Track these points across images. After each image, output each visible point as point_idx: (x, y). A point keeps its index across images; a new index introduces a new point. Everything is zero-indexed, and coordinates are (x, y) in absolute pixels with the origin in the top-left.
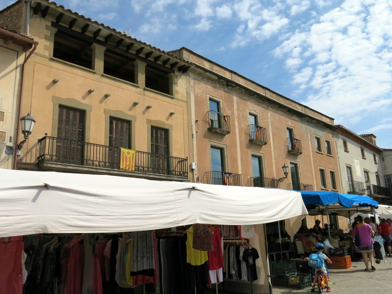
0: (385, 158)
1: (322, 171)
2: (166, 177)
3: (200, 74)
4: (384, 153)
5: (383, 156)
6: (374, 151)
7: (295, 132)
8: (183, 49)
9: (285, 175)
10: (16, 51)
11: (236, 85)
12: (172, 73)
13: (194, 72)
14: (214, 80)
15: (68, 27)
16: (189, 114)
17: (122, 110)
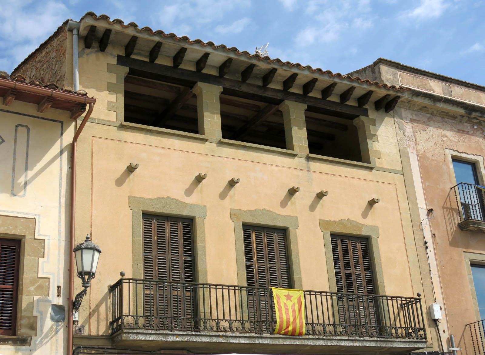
2: (376, 343)
3: (423, 109)
10: (59, 122)
12: (363, 115)
13: (410, 106)
15: (147, 60)
16: (411, 198)
17: (267, 208)
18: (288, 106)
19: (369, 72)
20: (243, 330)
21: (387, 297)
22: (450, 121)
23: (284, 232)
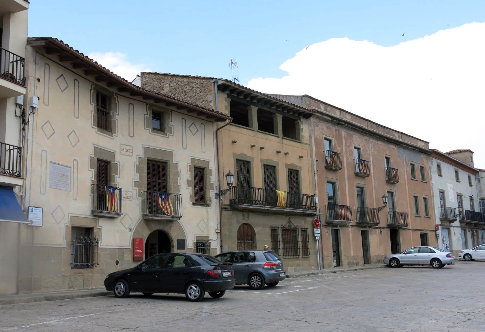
4: (480, 173)
5: (479, 176)
9: (384, 205)
15: (236, 96)
18: (277, 116)
19: (299, 98)
20: (263, 204)
22: (326, 122)
23: (275, 167)
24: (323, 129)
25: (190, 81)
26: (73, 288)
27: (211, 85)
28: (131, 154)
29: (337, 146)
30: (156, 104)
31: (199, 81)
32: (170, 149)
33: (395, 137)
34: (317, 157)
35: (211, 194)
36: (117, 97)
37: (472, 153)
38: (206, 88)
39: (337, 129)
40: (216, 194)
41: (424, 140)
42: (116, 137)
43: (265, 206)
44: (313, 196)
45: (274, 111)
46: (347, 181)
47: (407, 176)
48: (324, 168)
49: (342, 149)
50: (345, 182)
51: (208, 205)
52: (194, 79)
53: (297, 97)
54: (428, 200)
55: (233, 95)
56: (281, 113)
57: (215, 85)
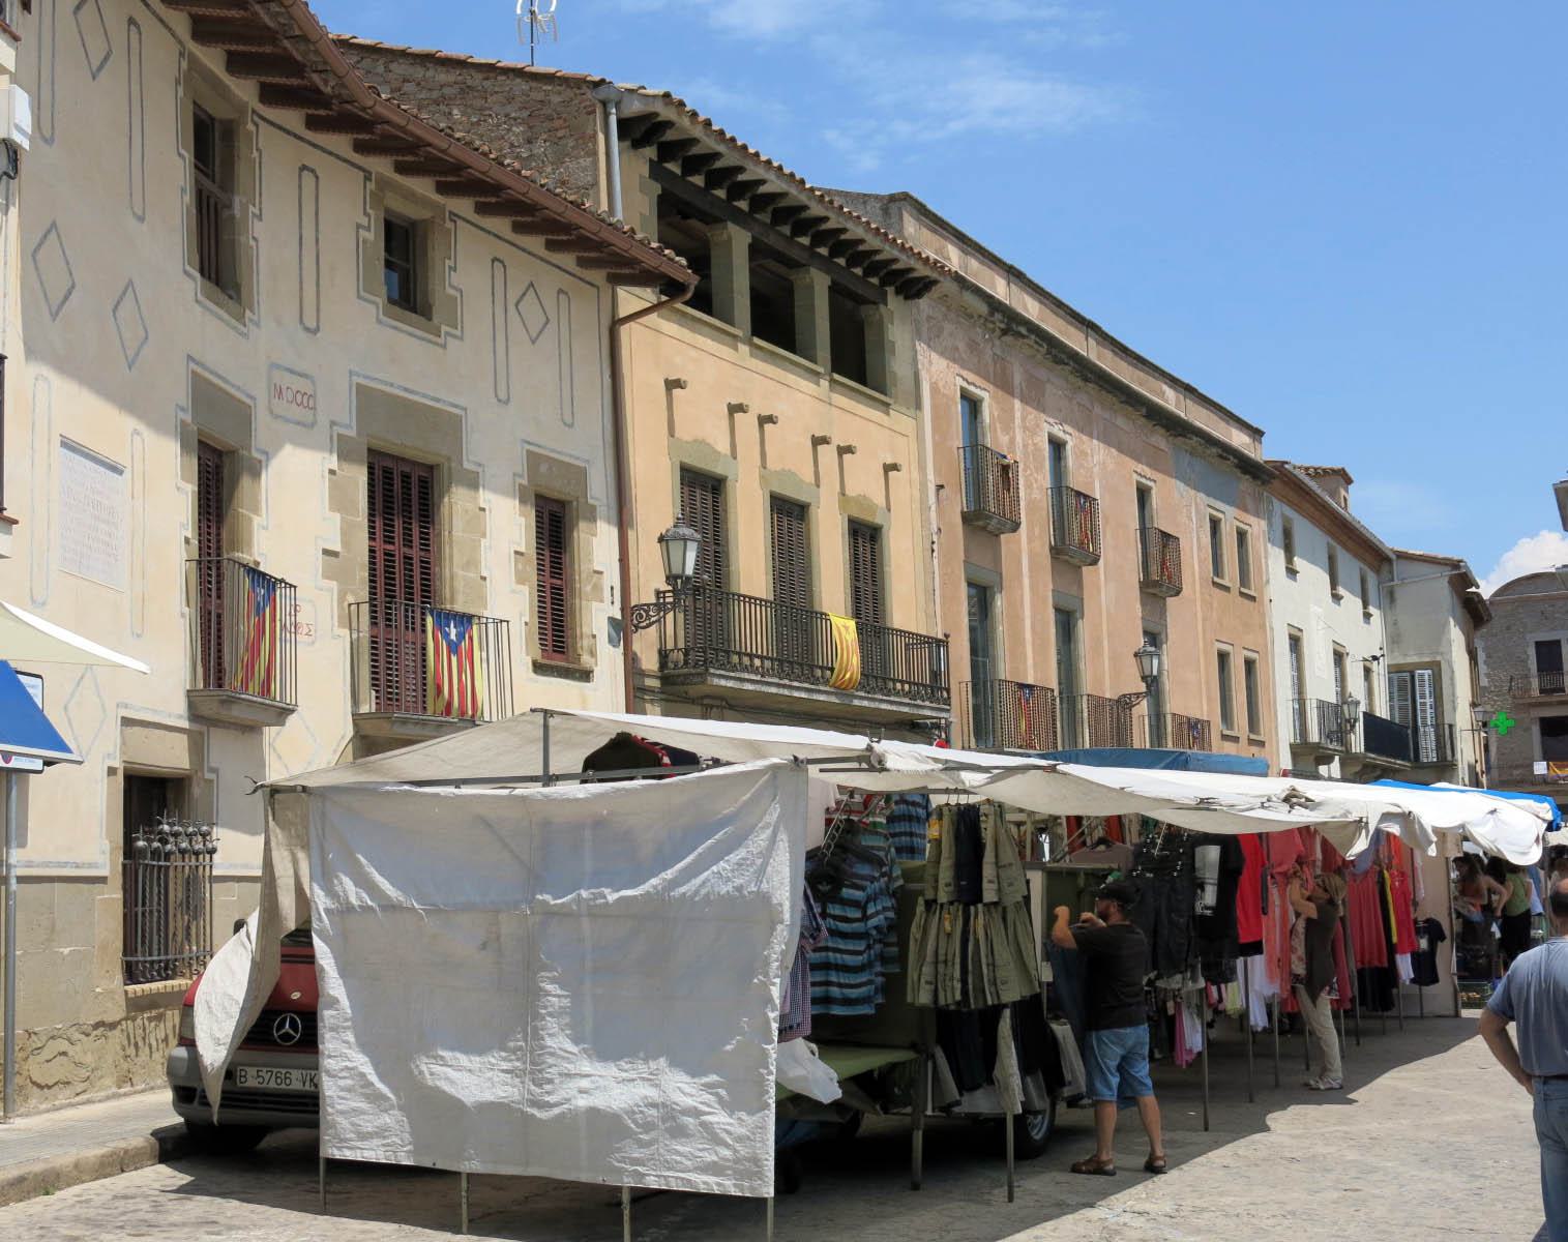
0: (1398, 595)
1: (1223, 657)
4: (1398, 567)
5: (1393, 580)
6: (1364, 561)
7: (1155, 499)
8: (905, 199)
9: (1144, 685)
11: (1029, 330)
14: (972, 317)
21: (739, 596)
24: (957, 349)
25: (469, 82)
26: (132, 1085)
27: (589, 113)
28: (308, 416)
29: (998, 425)
30: (398, 178)
31: (521, 85)
32: (451, 400)
33: (1167, 401)
34: (937, 472)
35: (596, 615)
36: (257, 125)
37: (1349, 481)
38: (561, 121)
39: (998, 353)
40: (612, 620)
41: (1250, 422)
42: (457, 342)
43: (796, 684)
44: (938, 642)
45: (801, 256)
46: (1026, 581)
47: (1200, 567)
48: (959, 520)
49: (1012, 441)
50: (1021, 588)
51: (585, 675)
52: (491, 75)
53: (865, 203)
54: (1259, 668)
55: (666, 169)
56: (826, 265)
57: (606, 115)
